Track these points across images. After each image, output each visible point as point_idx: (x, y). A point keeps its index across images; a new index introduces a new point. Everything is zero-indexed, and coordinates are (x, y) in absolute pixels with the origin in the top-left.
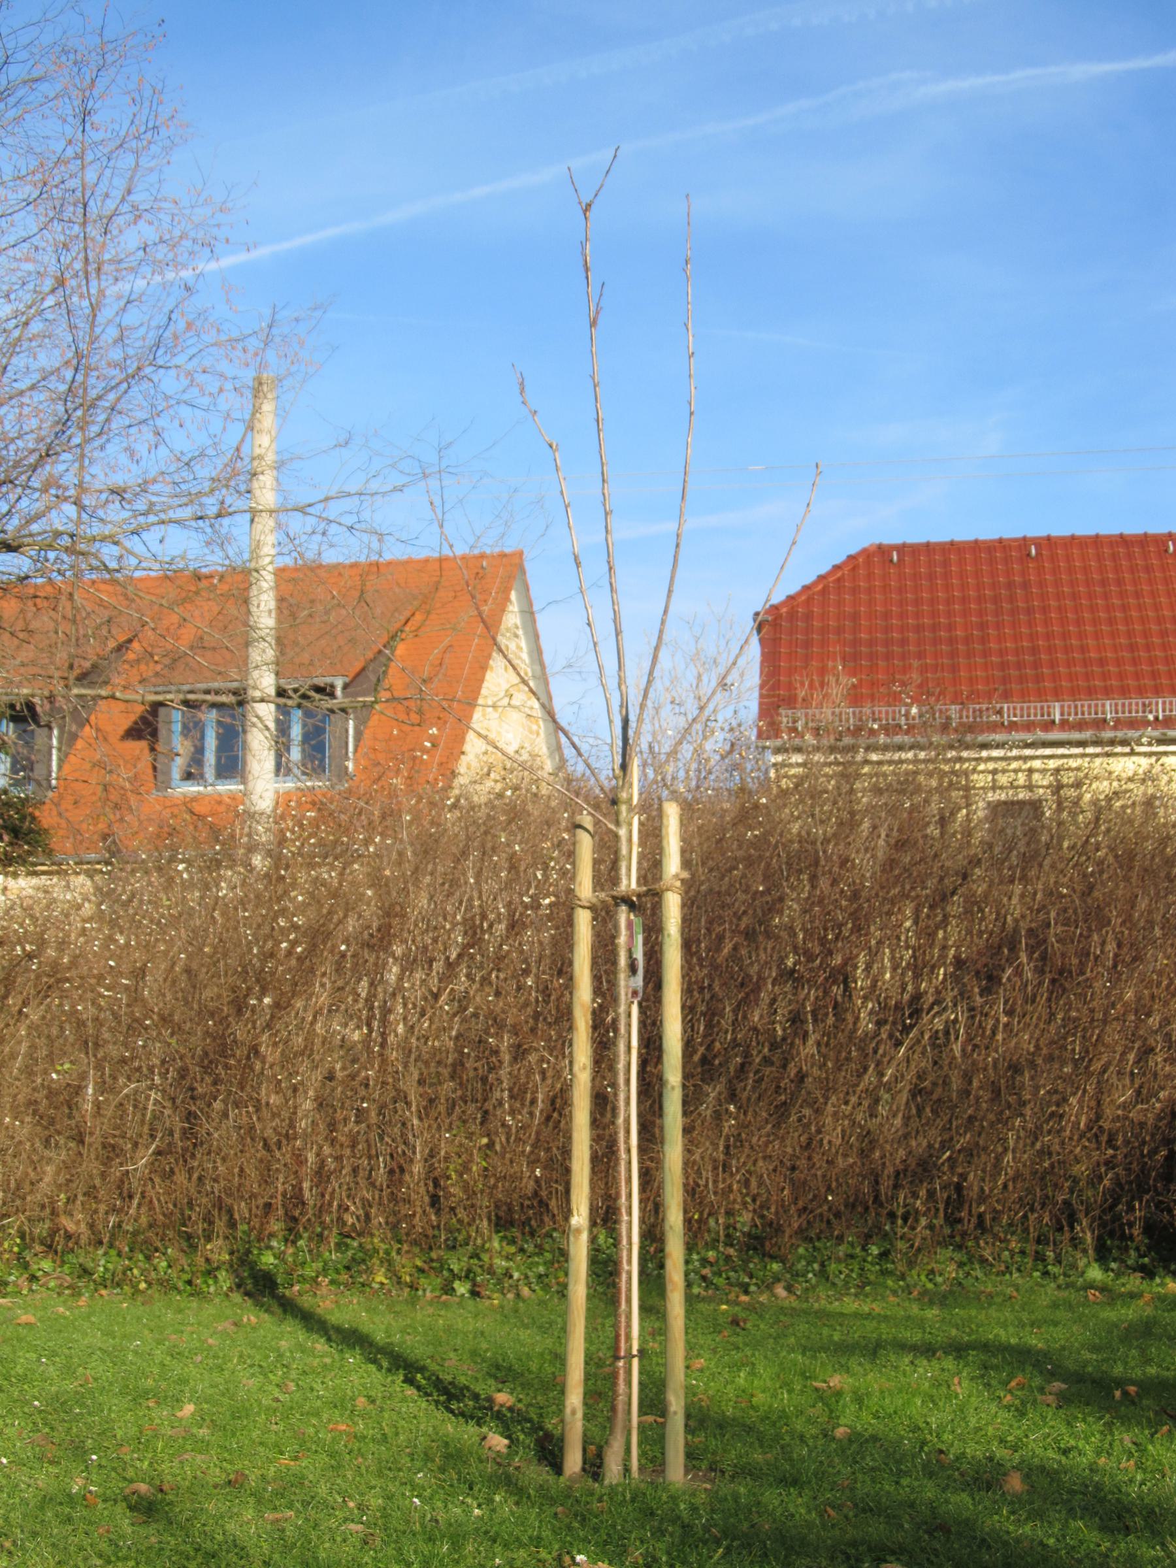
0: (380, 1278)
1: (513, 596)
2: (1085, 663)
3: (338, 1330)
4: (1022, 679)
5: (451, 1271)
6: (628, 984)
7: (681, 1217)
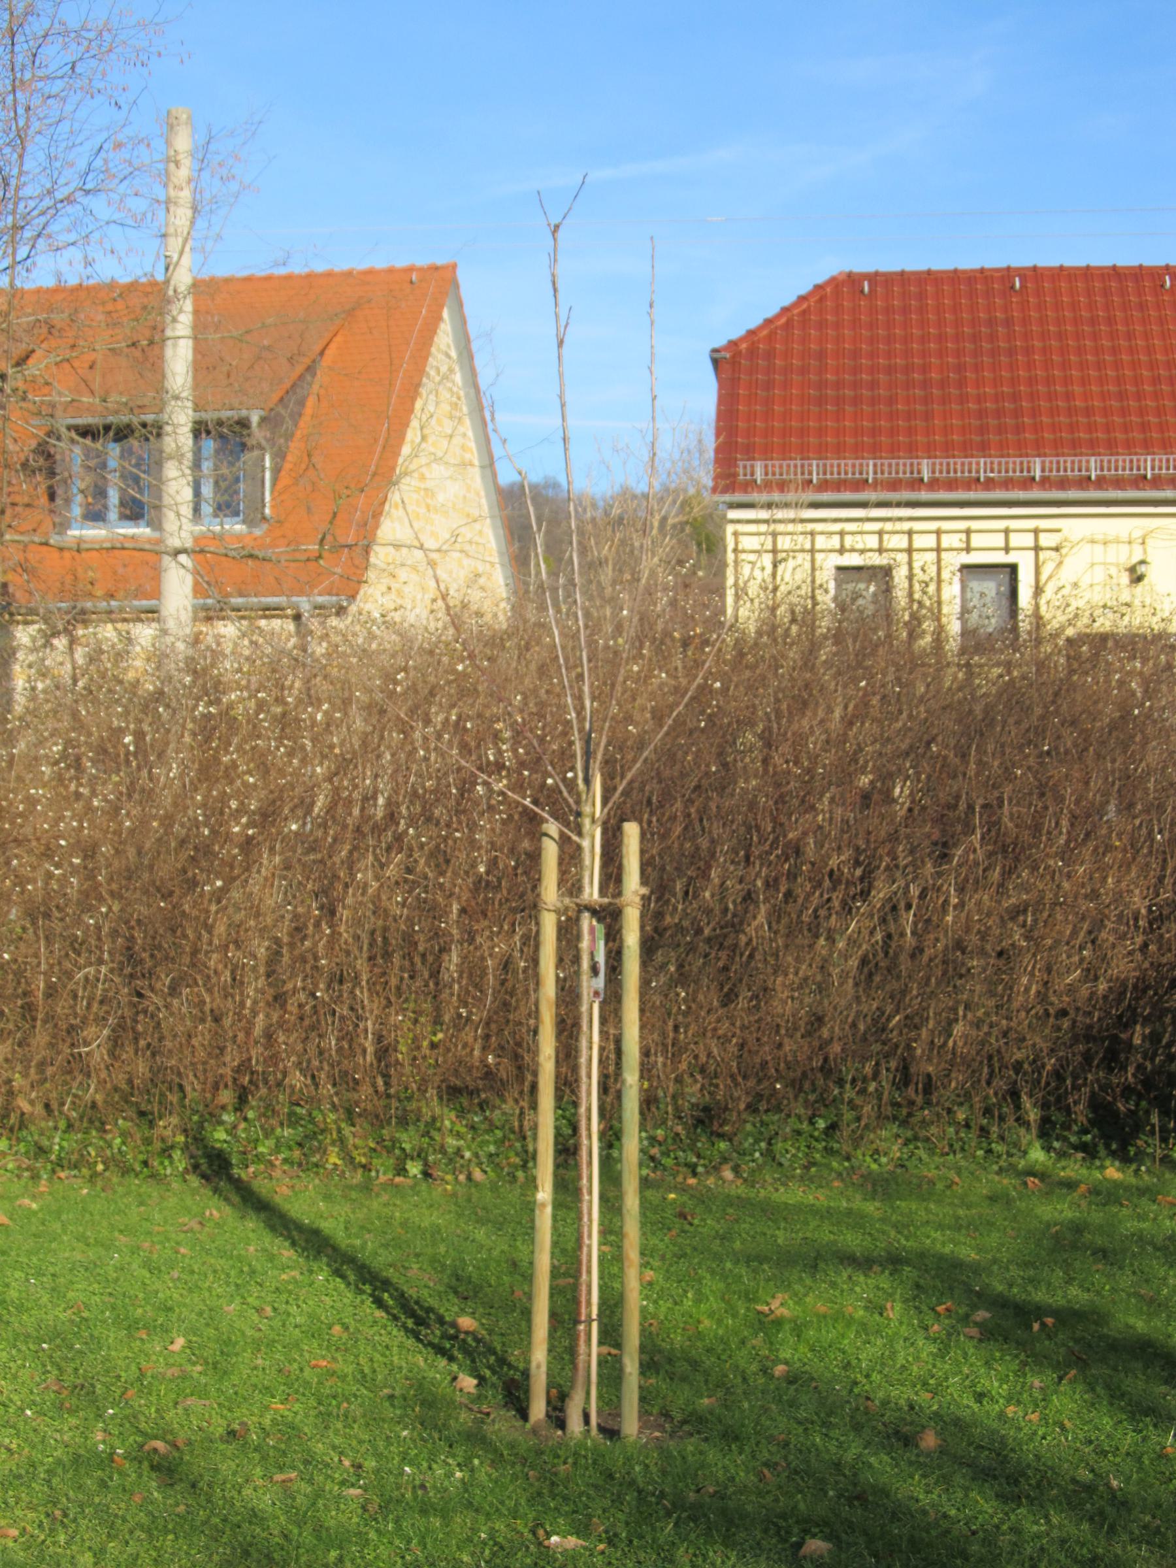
0: (334, 1159)
1: (446, 314)
2: (1070, 412)
3: (300, 1227)
4: (1000, 430)
5: (403, 1150)
6: (591, 986)
7: (637, 1202)
